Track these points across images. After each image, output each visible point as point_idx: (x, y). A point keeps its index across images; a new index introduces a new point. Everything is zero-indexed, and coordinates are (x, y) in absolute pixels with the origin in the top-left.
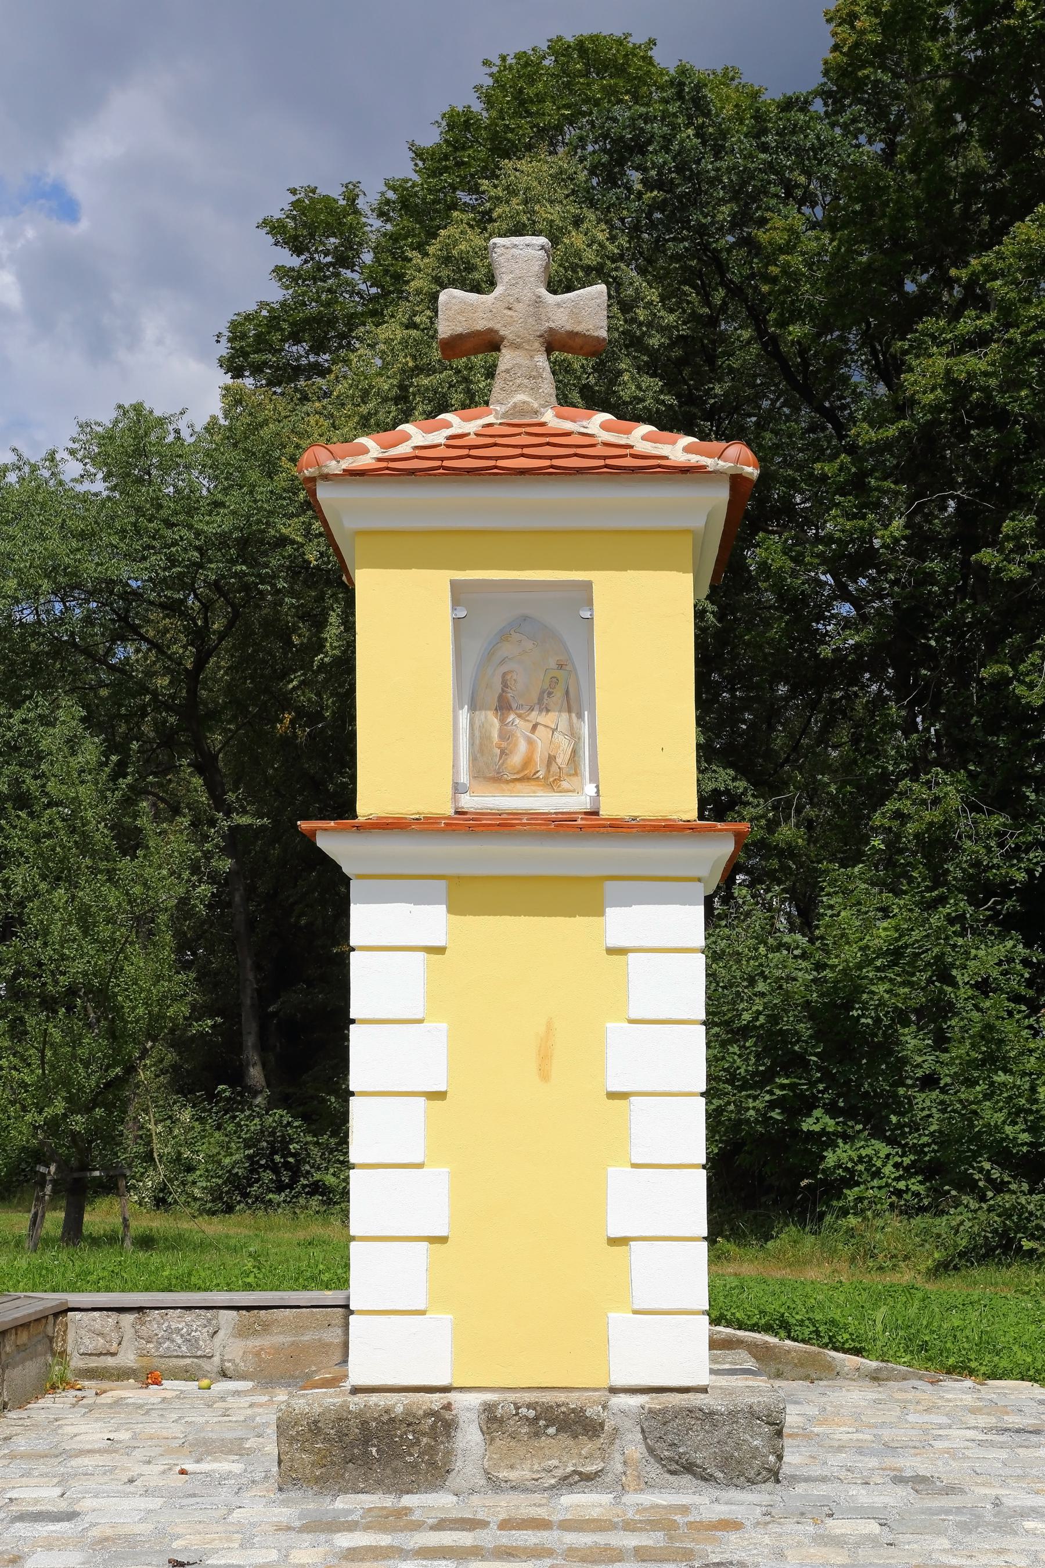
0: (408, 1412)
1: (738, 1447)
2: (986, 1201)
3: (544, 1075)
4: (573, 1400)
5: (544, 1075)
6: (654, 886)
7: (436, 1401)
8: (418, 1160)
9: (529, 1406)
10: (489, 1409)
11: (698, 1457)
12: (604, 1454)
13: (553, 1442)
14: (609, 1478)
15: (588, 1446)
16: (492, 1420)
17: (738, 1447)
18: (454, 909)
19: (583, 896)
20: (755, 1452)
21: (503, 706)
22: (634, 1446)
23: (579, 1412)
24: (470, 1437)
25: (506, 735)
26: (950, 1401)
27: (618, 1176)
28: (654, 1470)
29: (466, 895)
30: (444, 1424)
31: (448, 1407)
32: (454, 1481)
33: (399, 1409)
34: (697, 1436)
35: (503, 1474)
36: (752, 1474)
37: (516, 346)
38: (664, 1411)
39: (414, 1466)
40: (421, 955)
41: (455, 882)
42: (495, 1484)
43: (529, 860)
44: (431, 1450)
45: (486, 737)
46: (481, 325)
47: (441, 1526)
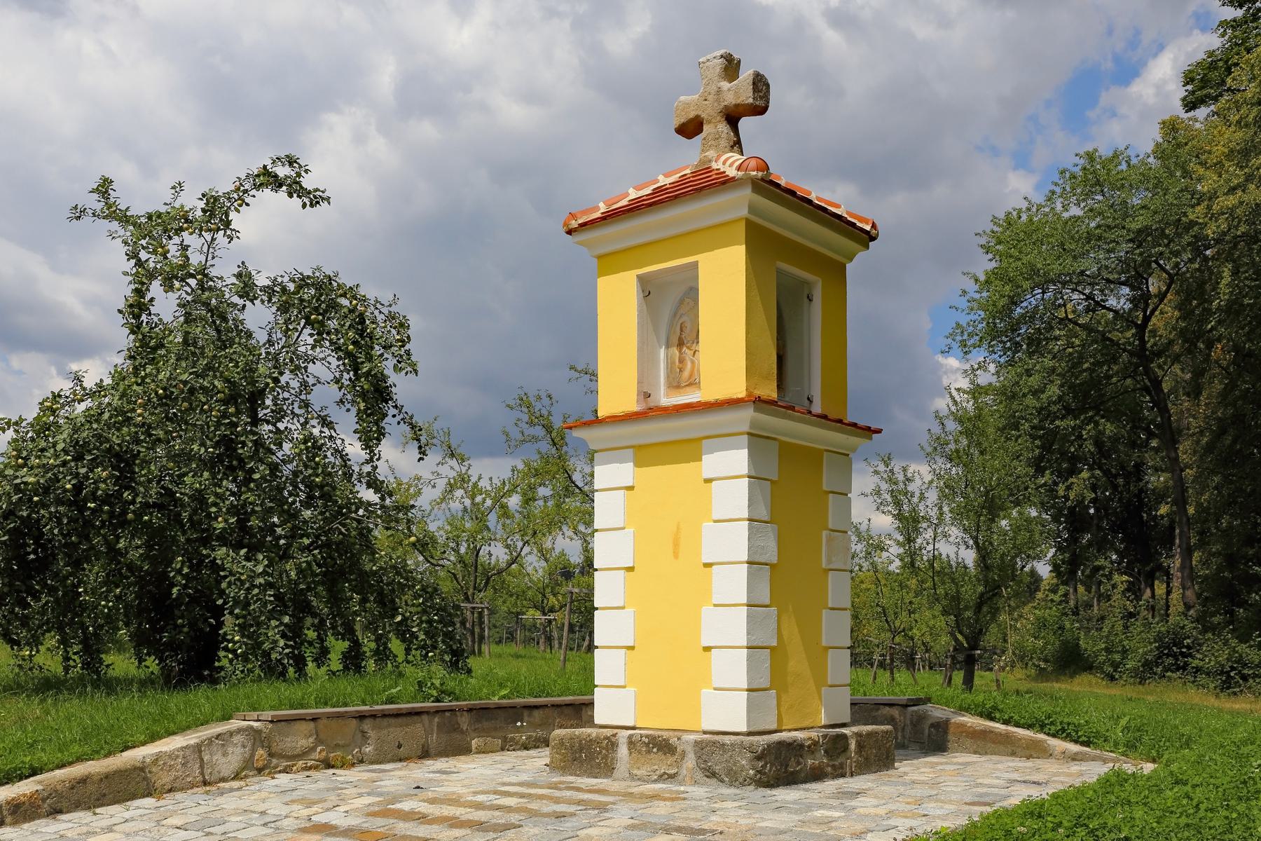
0: (597, 737)
1: (735, 764)
2: (228, 511)
3: (676, 556)
4: (665, 735)
5: (676, 556)
6: (722, 438)
7: (609, 732)
8: (621, 604)
9: (647, 736)
10: (630, 737)
11: (717, 768)
12: (678, 763)
13: (656, 756)
14: (680, 778)
15: (671, 760)
16: (631, 743)
17: (735, 764)
18: (638, 464)
19: (689, 450)
20: (742, 768)
21: (681, 344)
22: (690, 761)
23: (666, 741)
24: (623, 751)
25: (681, 361)
26: (998, 778)
27: (707, 611)
28: (699, 775)
29: (644, 455)
30: (612, 744)
31: (614, 735)
32: (616, 774)
33: (594, 735)
34: (716, 757)
35: (635, 772)
36: (741, 780)
37: (709, 122)
38: (702, 742)
39: (599, 764)
40: (622, 492)
41: (638, 448)
42: (632, 777)
43: (667, 431)
44: (605, 757)
45: (673, 363)
46: (692, 115)
47: (590, 791)
